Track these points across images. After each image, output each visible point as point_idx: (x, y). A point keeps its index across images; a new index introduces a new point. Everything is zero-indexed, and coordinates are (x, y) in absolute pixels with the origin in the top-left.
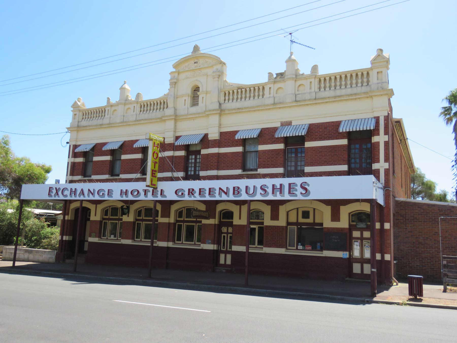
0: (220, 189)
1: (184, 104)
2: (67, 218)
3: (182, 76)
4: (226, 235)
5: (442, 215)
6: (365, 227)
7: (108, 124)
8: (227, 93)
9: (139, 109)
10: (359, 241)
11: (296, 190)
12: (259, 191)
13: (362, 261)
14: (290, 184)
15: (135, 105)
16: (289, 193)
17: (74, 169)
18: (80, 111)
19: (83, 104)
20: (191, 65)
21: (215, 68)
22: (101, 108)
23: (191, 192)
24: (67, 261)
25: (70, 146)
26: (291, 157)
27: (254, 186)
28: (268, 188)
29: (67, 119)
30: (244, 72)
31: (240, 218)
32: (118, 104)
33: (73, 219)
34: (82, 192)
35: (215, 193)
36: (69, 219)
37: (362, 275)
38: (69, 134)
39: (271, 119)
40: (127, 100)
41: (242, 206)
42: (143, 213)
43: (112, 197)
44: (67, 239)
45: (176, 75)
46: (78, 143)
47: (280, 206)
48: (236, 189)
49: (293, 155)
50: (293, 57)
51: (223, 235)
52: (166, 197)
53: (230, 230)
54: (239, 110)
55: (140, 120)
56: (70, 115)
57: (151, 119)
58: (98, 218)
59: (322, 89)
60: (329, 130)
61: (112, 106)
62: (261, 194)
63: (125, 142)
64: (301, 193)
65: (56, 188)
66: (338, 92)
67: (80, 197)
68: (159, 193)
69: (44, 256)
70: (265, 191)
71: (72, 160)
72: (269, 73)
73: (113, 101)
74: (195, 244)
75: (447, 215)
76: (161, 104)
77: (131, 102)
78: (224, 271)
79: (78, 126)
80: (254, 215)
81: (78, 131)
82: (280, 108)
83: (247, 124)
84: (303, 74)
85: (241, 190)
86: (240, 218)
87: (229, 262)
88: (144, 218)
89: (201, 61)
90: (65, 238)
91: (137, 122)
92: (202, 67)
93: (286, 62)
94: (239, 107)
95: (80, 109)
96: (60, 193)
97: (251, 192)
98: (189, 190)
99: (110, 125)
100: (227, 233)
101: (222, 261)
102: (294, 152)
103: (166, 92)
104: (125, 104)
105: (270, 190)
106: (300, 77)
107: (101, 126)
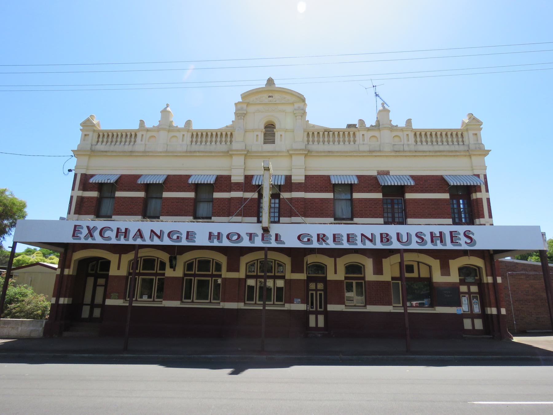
0: (362, 235)
1: (256, 140)
2: (66, 272)
3: (251, 109)
4: (314, 292)
5: (509, 271)
6: (473, 281)
7: (143, 152)
8: (311, 134)
9: (96, 140)
10: (467, 296)
11: (460, 239)
12: (414, 239)
13: (472, 316)
14: (451, 233)
15: (185, 133)
16: (452, 241)
17: (80, 207)
18: (94, 131)
19: (98, 124)
20: (264, 98)
21: (296, 106)
22: (131, 131)
23: (322, 239)
24: (66, 334)
25: (76, 175)
26: (387, 208)
27: (407, 233)
28: (425, 235)
29: (75, 139)
30: (323, 113)
31: (336, 273)
32: (157, 129)
33: (75, 274)
34: (140, 233)
35: (343, 240)
36: (71, 273)
37: (474, 331)
38: (75, 160)
39: (369, 167)
40: (171, 125)
41: (338, 259)
42: (196, 266)
43: (194, 242)
44: (66, 302)
45: (245, 106)
46: (90, 172)
47: (383, 260)
48: (384, 236)
49: (389, 206)
50: (168, 109)
51: (310, 292)
52: (284, 243)
53: (320, 286)
54: (330, 154)
55: (195, 152)
56: (78, 135)
57: (211, 152)
58: (123, 272)
59: (419, 143)
60: (438, 183)
61: (148, 130)
62: (417, 242)
63: (168, 176)
64: (466, 243)
65: (88, 227)
66: (436, 148)
67: (135, 240)
68: (273, 238)
69: (20, 329)
70: (423, 239)
71: (81, 193)
72: (141, 121)
73: (148, 125)
74: (274, 304)
75: (513, 271)
76: (224, 136)
77: (179, 130)
78: (320, 335)
79: (92, 151)
80: (354, 269)
81: (90, 156)
82: (376, 156)
83: (343, 168)
84: (397, 126)
85: (391, 238)
86: (336, 273)
87: (321, 324)
88: (197, 273)
89: (277, 96)
90: (62, 301)
91: (189, 154)
92: (277, 102)
93: (162, 112)
94: (330, 150)
95: (95, 129)
96: (96, 234)
97: (405, 239)
98: (318, 235)
99: (146, 154)
100: (316, 290)
101: (312, 324)
102: (394, 201)
103: (230, 123)
104: (169, 131)
105: (428, 238)
106: (395, 128)
107: (131, 154)
